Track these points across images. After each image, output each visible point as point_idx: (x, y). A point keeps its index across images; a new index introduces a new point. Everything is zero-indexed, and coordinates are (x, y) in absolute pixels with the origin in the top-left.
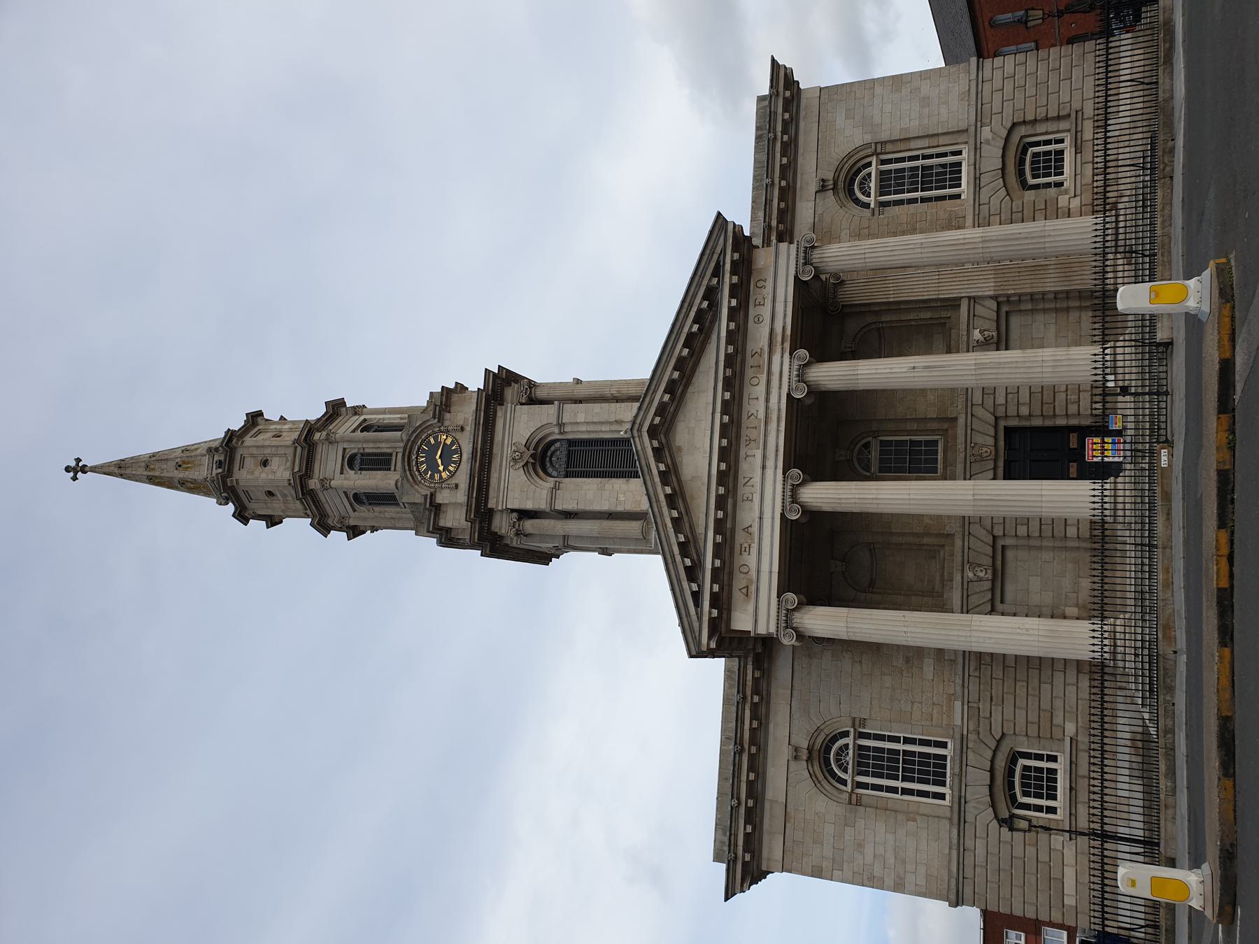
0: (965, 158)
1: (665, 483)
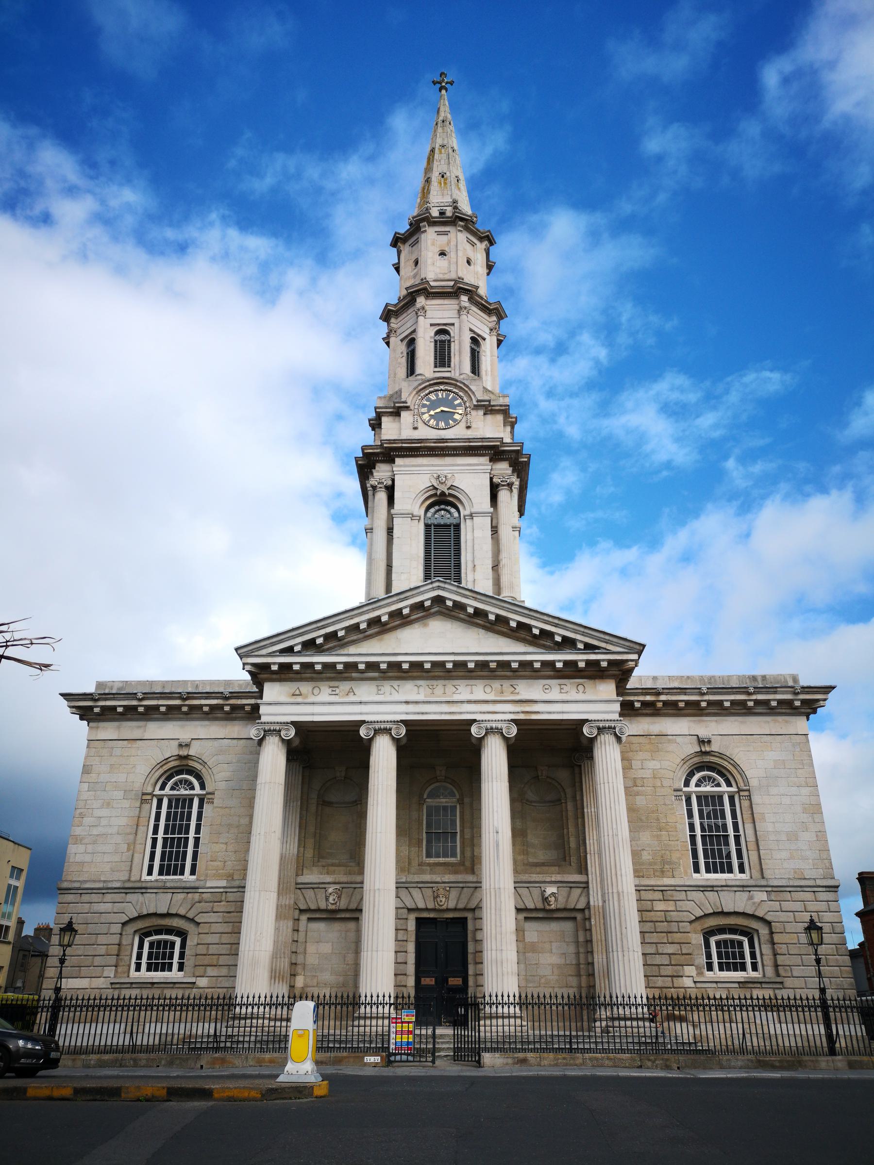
0: (736, 876)
1: (392, 615)
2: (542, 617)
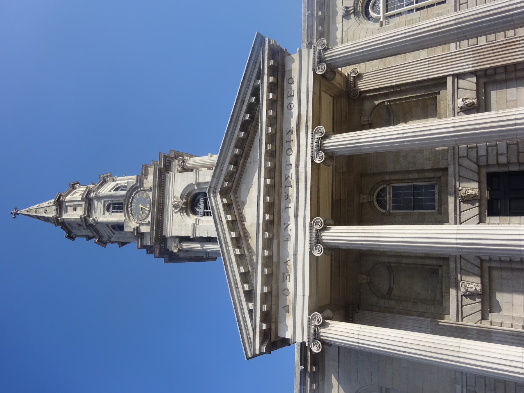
2: (236, 112)
